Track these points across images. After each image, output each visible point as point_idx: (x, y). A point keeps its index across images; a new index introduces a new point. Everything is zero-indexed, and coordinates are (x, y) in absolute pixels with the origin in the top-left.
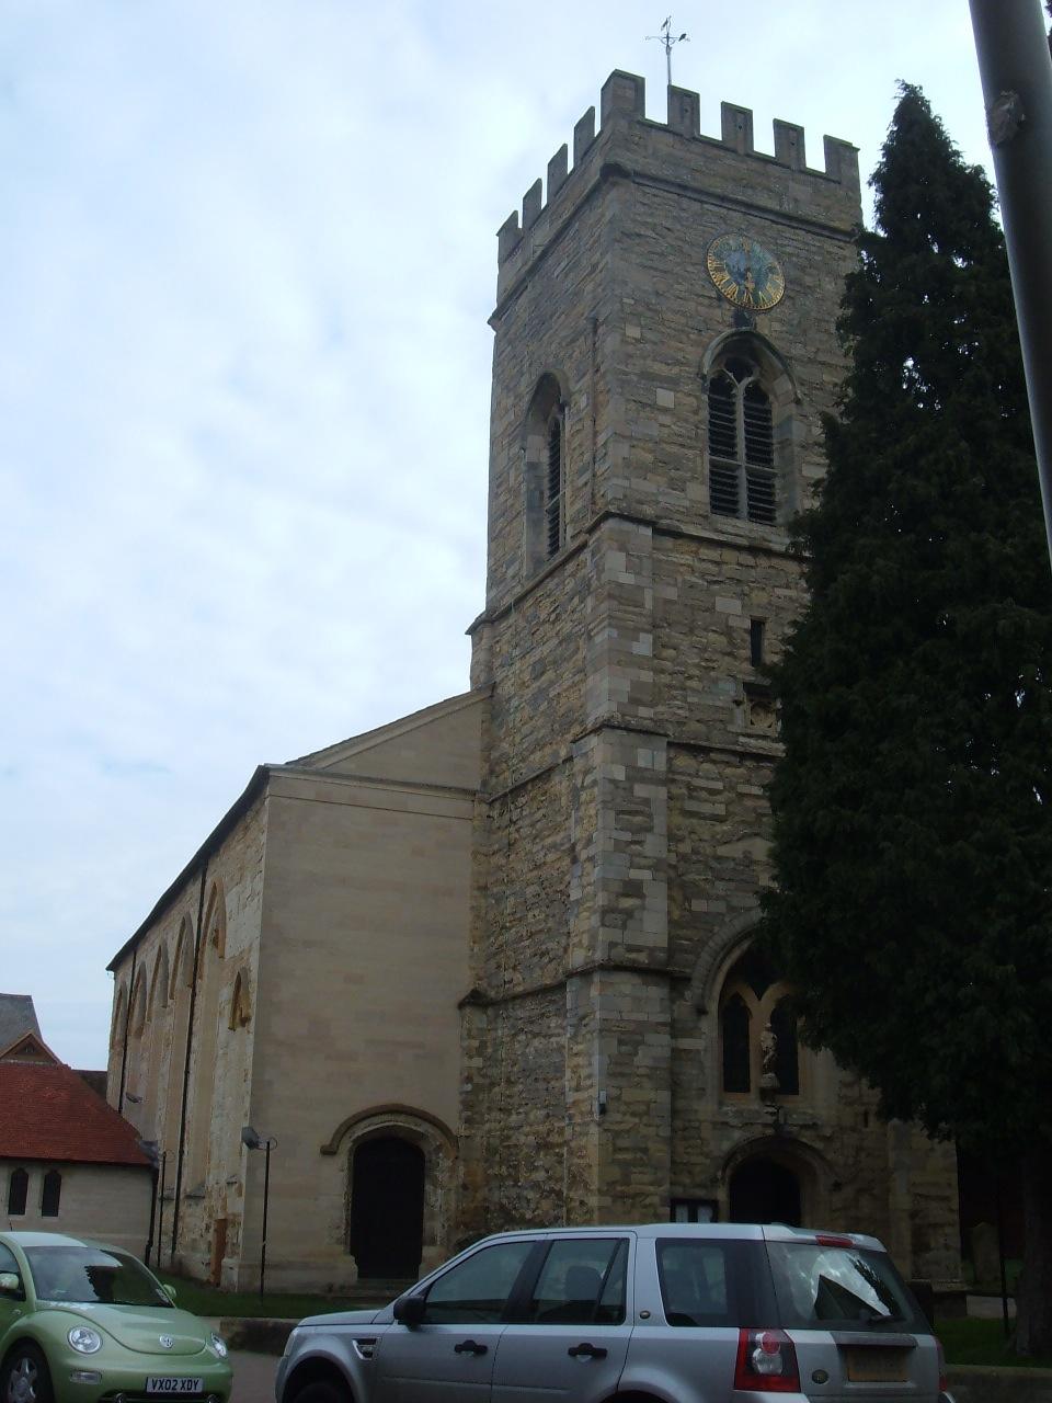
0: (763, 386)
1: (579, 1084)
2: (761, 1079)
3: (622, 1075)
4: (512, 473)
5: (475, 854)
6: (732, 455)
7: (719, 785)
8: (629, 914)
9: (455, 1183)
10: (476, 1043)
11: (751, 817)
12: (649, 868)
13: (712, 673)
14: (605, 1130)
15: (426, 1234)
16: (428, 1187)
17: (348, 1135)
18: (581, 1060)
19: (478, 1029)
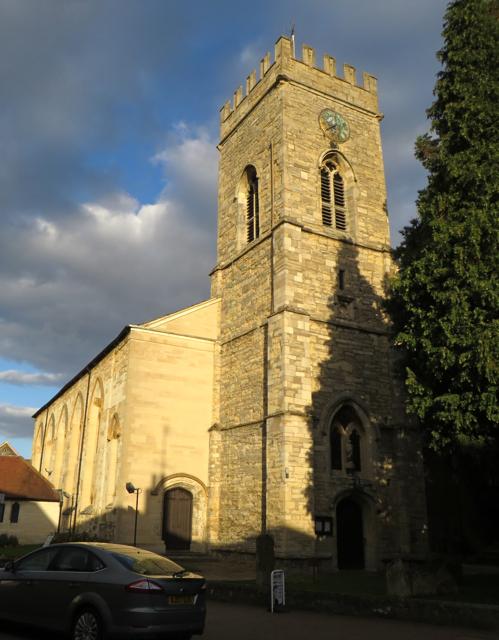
2: (346, 464)
3: (294, 461)
4: (230, 209)
6: (329, 201)
16: (195, 510)
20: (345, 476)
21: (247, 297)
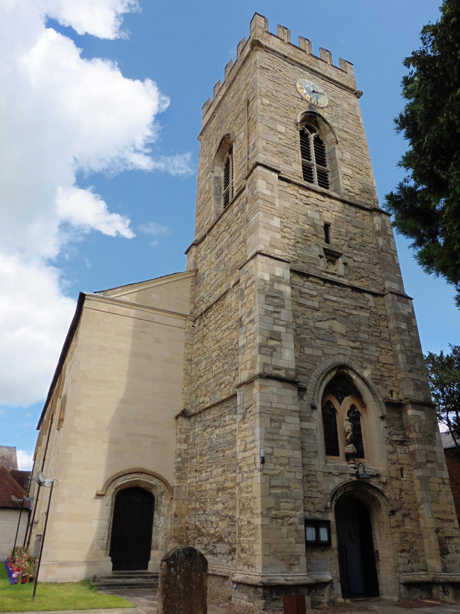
0: (321, 137)
1: (246, 447)
5: (186, 344)
7: (315, 293)
8: (274, 349)
9: (170, 513)
10: (184, 436)
11: (331, 310)
12: (283, 326)
13: (308, 243)
14: (264, 474)
15: (153, 544)
16: (156, 516)
17: (113, 484)
18: (247, 433)
19: (185, 429)
20: (344, 464)
21: (220, 261)
